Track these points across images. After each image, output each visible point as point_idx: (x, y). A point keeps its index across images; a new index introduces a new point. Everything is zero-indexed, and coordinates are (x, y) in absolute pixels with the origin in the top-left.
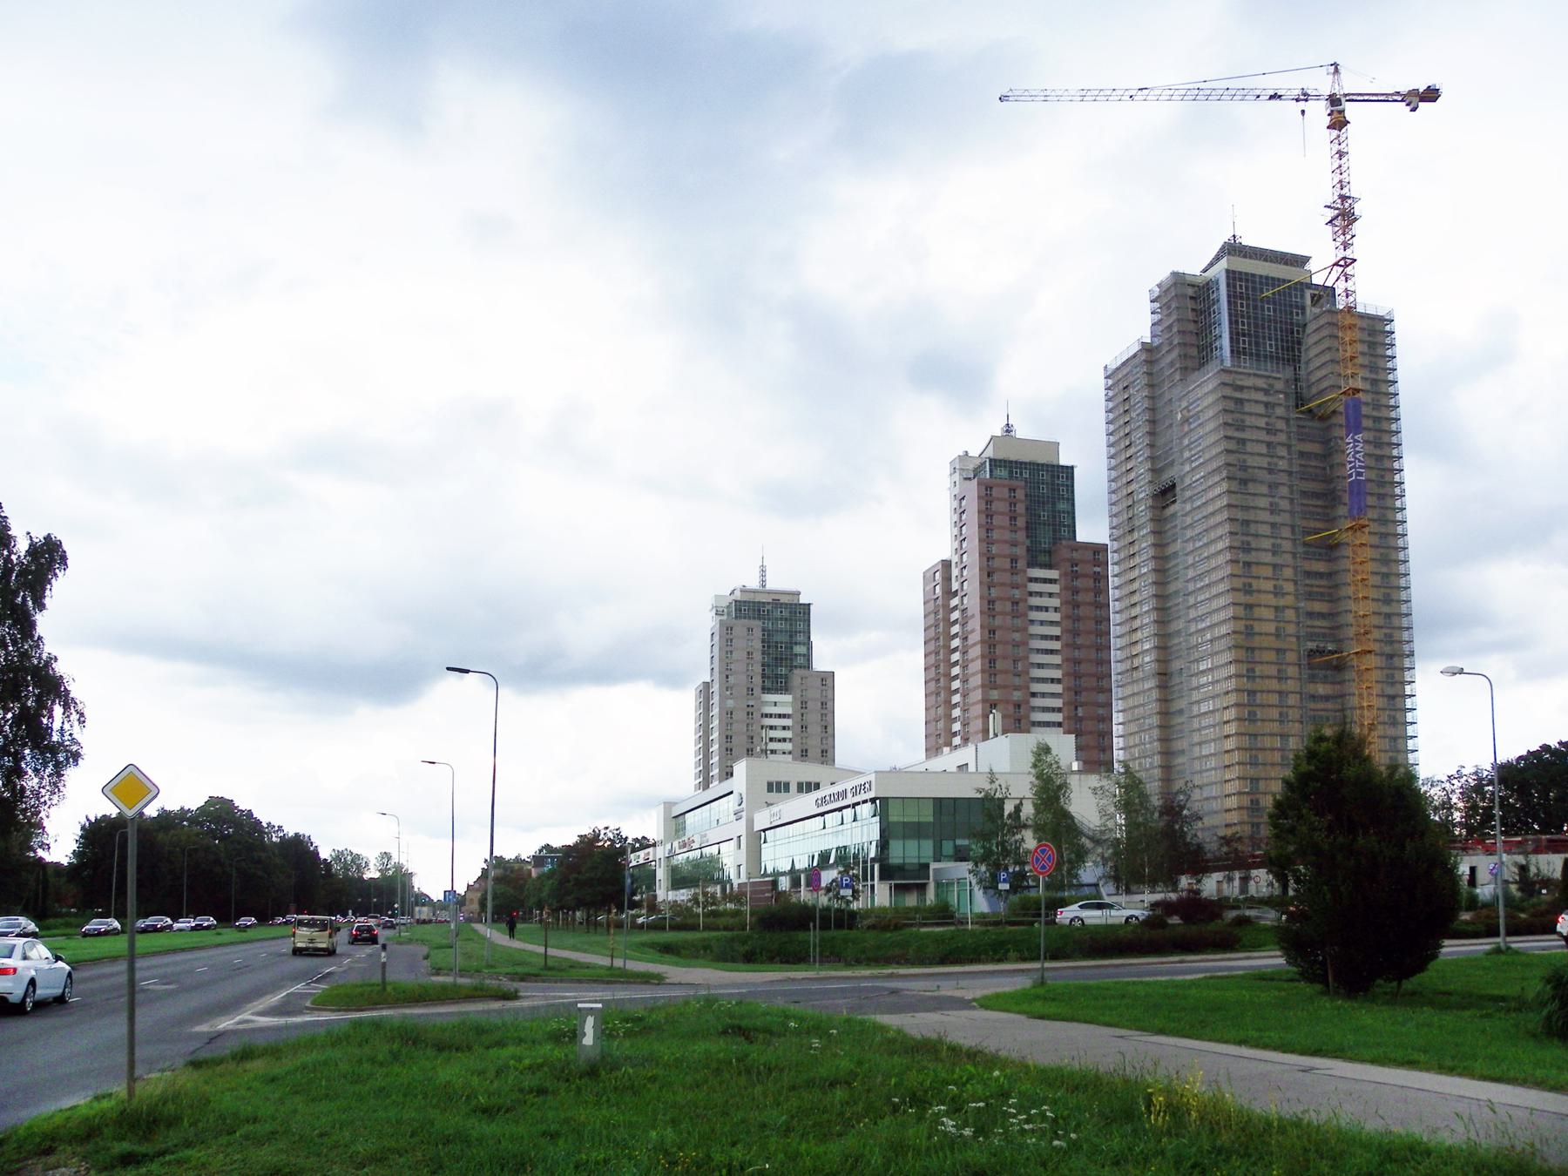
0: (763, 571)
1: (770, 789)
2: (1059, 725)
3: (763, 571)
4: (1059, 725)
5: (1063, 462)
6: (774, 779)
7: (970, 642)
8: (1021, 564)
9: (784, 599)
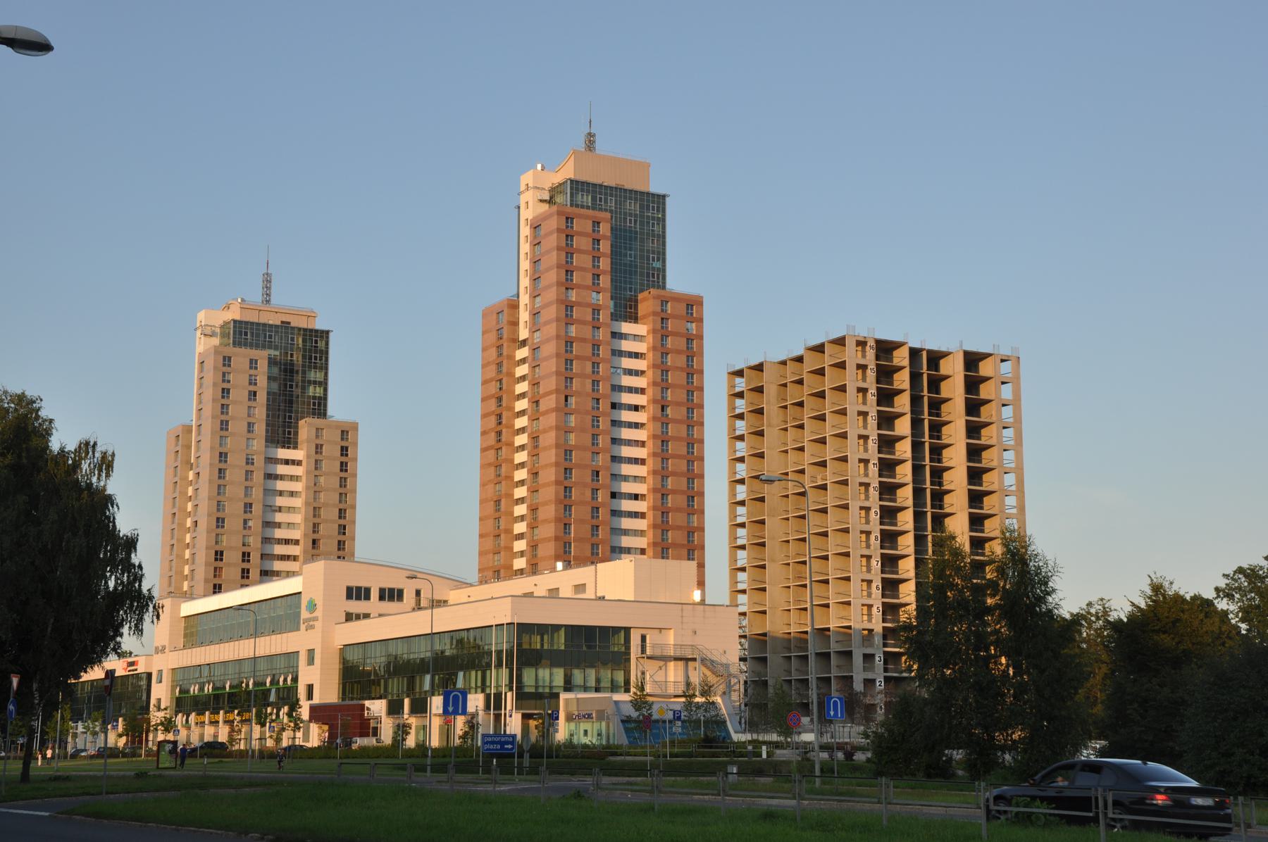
0: (267, 280)
1: (349, 596)
2: (643, 551)
3: (267, 280)
4: (643, 551)
5: (654, 189)
6: (354, 584)
7: (542, 407)
8: (604, 317)
9: (296, 322)
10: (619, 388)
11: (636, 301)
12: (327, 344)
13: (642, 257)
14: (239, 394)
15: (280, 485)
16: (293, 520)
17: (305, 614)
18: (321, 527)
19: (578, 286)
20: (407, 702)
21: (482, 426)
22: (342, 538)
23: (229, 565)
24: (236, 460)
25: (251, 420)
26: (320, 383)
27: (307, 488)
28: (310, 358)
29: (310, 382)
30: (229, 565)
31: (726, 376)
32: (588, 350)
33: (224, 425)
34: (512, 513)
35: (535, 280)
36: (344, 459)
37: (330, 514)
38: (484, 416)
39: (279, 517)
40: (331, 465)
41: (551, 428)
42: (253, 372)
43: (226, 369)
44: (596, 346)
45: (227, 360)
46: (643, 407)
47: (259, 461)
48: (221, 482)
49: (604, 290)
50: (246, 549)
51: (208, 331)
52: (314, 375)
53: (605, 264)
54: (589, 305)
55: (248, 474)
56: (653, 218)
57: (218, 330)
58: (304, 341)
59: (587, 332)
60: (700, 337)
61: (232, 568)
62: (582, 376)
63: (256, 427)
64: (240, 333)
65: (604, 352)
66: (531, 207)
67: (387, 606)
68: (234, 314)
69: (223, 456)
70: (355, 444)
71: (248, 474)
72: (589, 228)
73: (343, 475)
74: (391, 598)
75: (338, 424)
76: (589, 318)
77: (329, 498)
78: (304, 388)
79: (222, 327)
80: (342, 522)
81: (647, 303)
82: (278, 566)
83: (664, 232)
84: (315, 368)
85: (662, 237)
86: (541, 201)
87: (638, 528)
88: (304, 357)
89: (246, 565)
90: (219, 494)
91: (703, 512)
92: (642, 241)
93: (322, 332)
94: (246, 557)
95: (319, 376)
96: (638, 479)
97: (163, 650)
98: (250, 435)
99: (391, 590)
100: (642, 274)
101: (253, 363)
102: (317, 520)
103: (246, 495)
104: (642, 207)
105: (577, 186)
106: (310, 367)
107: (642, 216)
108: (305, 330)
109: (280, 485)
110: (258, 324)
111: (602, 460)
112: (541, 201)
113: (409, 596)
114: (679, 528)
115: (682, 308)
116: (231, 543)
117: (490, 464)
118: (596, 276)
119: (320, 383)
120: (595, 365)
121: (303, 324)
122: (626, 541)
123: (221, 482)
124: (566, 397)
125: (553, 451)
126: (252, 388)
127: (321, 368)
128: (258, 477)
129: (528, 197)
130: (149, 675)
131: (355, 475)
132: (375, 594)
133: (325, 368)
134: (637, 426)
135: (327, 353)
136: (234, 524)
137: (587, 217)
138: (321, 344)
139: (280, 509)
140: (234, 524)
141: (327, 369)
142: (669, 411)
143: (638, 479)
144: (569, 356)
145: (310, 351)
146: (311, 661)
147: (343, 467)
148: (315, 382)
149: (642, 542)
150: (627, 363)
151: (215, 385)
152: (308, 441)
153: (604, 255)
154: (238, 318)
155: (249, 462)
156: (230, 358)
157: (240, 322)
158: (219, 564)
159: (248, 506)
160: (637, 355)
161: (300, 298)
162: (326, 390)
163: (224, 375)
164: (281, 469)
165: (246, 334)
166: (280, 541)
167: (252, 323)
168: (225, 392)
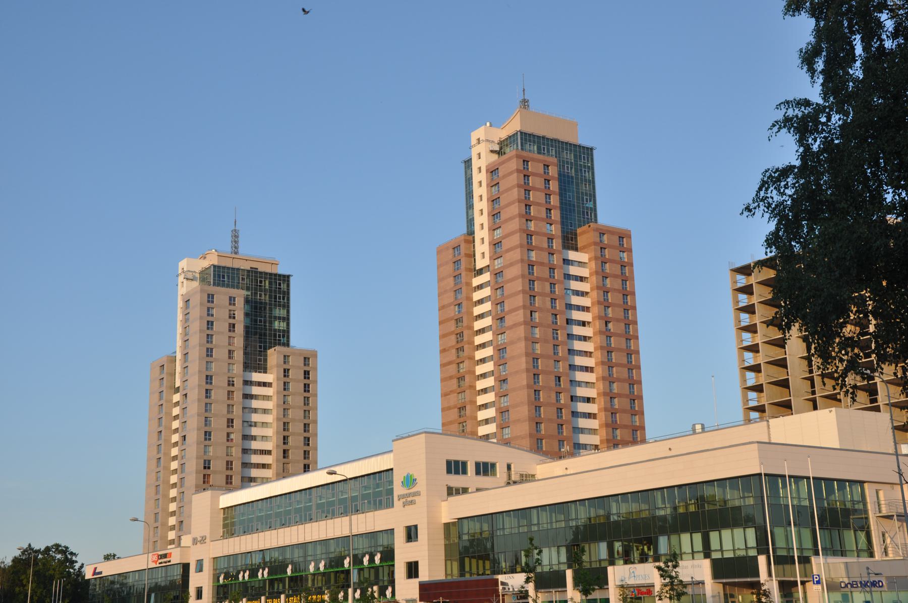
0: (235, 236)
1: (449, 471)
3: (235, 236)
9: (262, 268)
10: (570, 307)
11: (576, 235)
12: (288, 286)
13: (578, 198)
14: (221, 326)
15: (255, 404)
16: (267, 434)
17: (398, 490)
18: (290, 439)
19: (536, 219)
20: (569, 574)
21: (441, 345)
22: (306, 448)
23: (215, 472)
24: (219, 382)
25: (231, 348)
26: (284, 319)
27: (278, 406)
28: (275, 298)
29: (275, 318)
30: (215, 472)
31: (729, 273)
32: (546, 273)
33: (209, 352)
34: (476, 417)
35: (494, 215)
36: (307, 381)
37: (296, 428)
38: (443, 336)
39: (254, 431)
40: (296, 387)
41: (519, 339)
42: (232, 307)
43: (210, 305)
44: (552, 269)
45: (211, 298)
46: (589, 323)
47: (238, 382)
48: (208, 401)
49: (556, 222)
50: (230, 459)
51: (190, 276)
52: (279, 312)
53: (555, 200)
54: (544, 234)
55: (230, 394)
56: (585, 167)
57: (198, 275)
58: (270, 283)
59: (544, 257)
60: (631, 264)
61: (218, 478)
62: (542, 294)
63: (235, 354)
64: (219, 276)
65: (558, 275)
66: (482, 159)
67: (483, 481)
68: (213, 260)
69: (209, 379)
70: (315, 369)
71: (230, 394)
72: (541, 170)
73: (306, 394)
74: (486, 473)
75: (300, 352)
76: (545, 245)
77: (296, 414)
78: (271, 323)
79: (201, 273)
80: (306, 435)
81: (585, 236)
82: (254, 473)
83: (593, 178)
84: (280, 306)
85: (592, 182)
86: (492, 151)
87: (592, 428)
88: (270, 297)
89: (229, 473)
90: (206, 411)
91: (642, 413)
92: (577, 185)
93: (284, 276)
94: (229, 465)
95: (283, 313)
96: (590, 385)
97: (203, 540)
98: (231, 361)
99: (485, 464)
100: (579, 213)
101: (232, 300)
102: (286, 433)
103: (228, 412)
104: (575, 156)
105: (526, 138)
106: (275, 305)
107: (576, 164)
108: (271, 274)
109: (255, 404)
110: (233, 269)
111: (562, 367)
112: (492, 151)
113: (500, 470)
114: (625, 427)
115: (615, 240)
116: (217, 452)
117: (451, 378)
118: (549, 210)
119: (284, 319)
120: (552, 285)
121: (268, 269)
122: (584, 439)
123: (208, 401)
124: (531, 312)
125: (524, 359)
126: (232, 321)
127: (284, 306)
128: (238, 396)
129: (483, 148)
130: (186, 567)
131: (316, 395)
132: (471, 468)
133: (287, 306)
134: (585, 339)
135: (288, 293)
136: (219, 436)
137: (539, 161)
138: (283, 286)
139: (255, 424)
140: (219, 436)
141: (288, 307)
142: (610, 326)
143: (590, 385)
144: (531, 277)
145: (275, 291)
146: (200, 569)
147: (306, 388)
148: (279, 318)
149: (595, 440)
150: (575, 285)
151: (201, 318)
152: (278, 366)
153: (554, 193)
154: (216, 263)
155: (231, 383)
156: (213, 295)
157: (219, 267)
158: (207, 472)
159: (230, 422)
160: (581, 279)
161: (261, 251)
162: (288, 325)
163: (208, 309)
164: (255, 390)
165: (223, 277)
166: (256, 452)
167: (228, 268)
168: (210, 324)
